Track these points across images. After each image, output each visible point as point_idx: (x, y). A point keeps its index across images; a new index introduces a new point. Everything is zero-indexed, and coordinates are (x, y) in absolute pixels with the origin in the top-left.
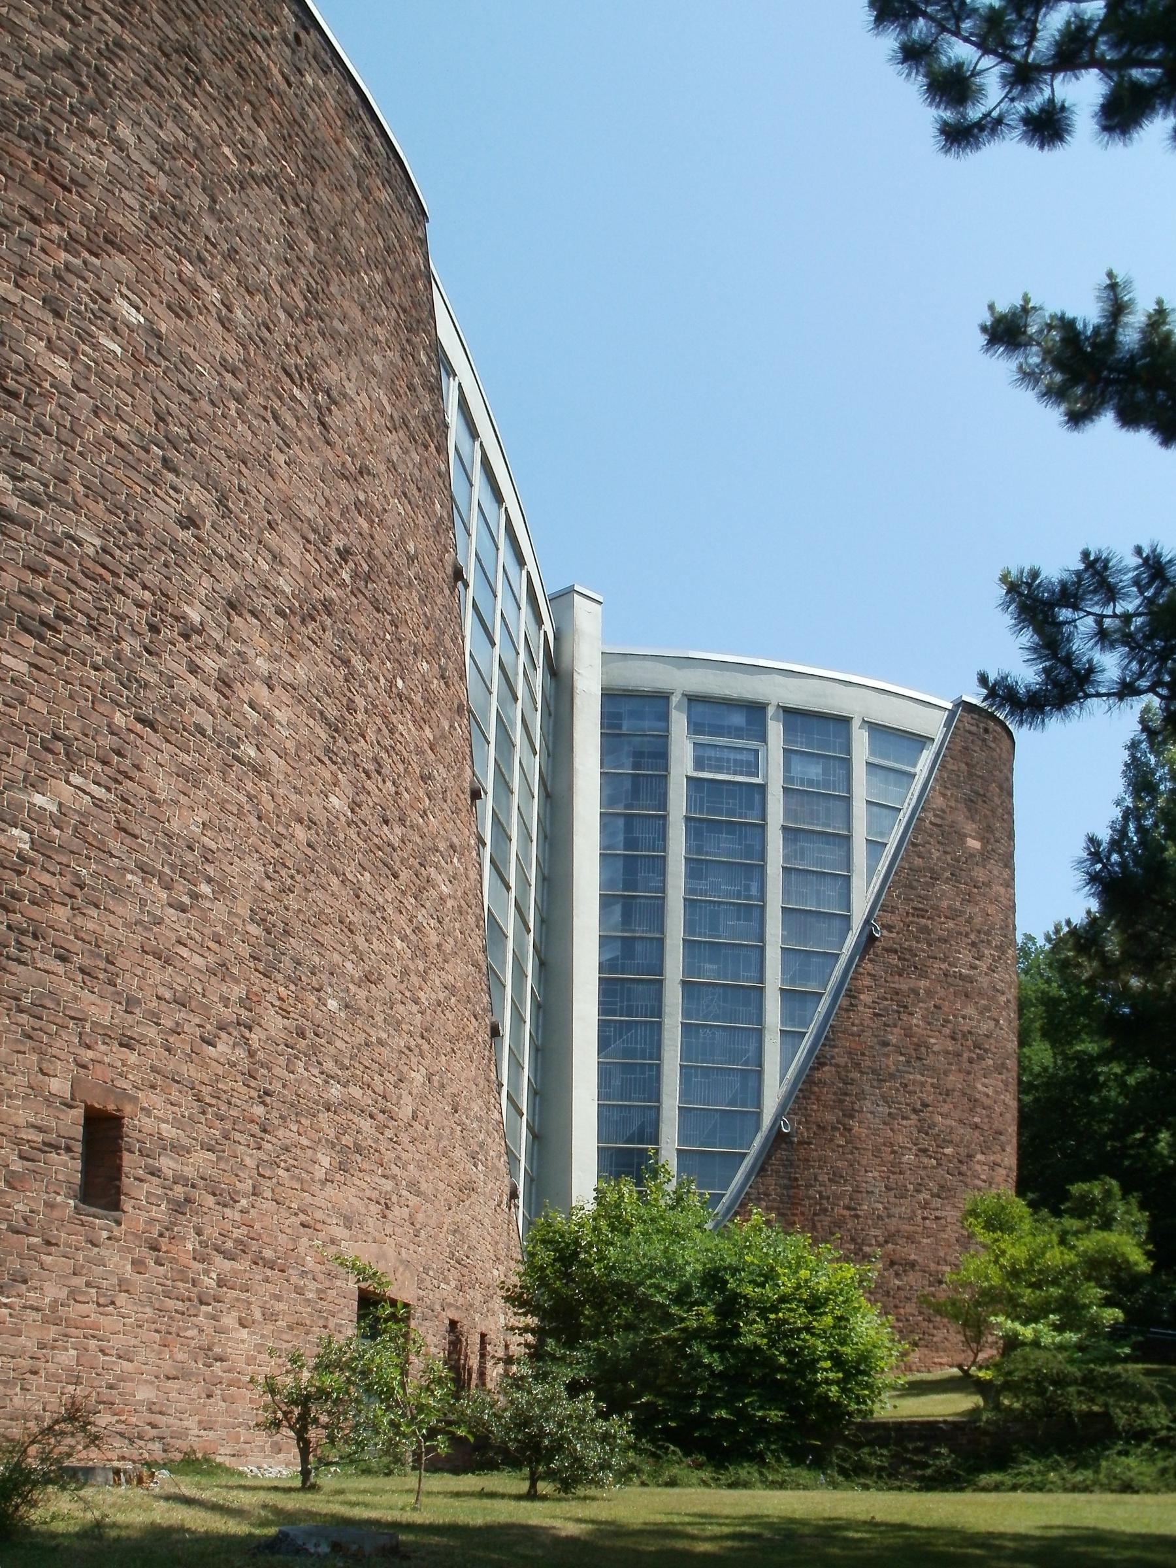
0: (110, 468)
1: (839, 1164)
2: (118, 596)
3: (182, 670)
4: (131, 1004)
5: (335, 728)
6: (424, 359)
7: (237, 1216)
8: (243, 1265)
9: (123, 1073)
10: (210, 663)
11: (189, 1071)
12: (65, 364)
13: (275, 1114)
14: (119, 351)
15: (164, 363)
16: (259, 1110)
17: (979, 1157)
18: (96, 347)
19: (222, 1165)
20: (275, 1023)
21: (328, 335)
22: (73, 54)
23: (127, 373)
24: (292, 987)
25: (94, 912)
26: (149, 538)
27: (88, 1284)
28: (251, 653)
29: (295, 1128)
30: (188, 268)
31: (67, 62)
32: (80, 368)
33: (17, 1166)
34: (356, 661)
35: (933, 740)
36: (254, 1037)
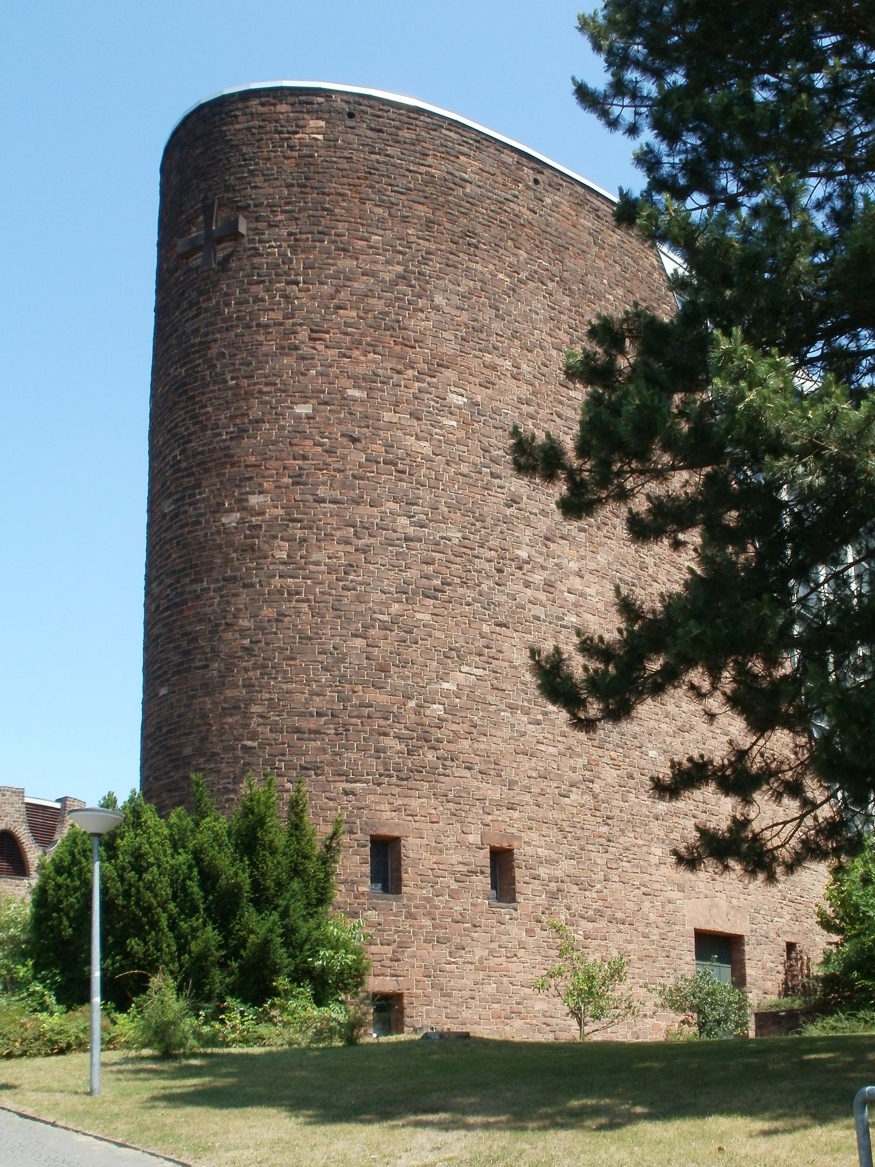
0: (460, 492)
2: (477, 561)
3: (520, 587)
4: (511, 785)
7: (595, 895)
8: (601, 924)
9: (510, 826)
10: (538, 578)
11: (552, 815)
12: (427, 444)
14: (455, 423)
15: (482, 418)
16: (605, 829)
19: (581, 866)
20: (610, 775)
22: (405, 271)
23: (461, 434)
24: (621, 750)
25: (484, 739)
26: (489, 521)
27: (500, 946)
29: (632, 835)
32: (435, 443)
33: (455, 886)
36: (596, 787)
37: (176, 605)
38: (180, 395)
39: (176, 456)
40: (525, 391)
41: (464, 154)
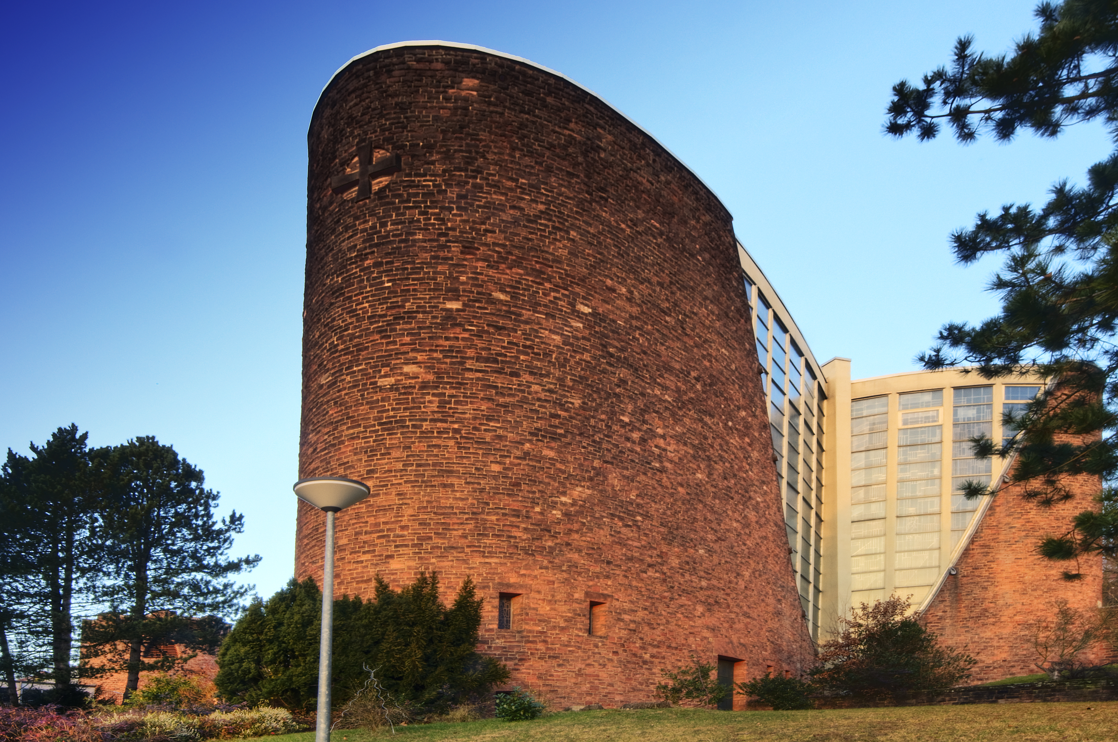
8: (663, 650)
10: (636, 435)
18: (571, 327)
20: (675, 562)
21: (683, 288)
28: (654, 429)
30: (609, 282)
34: (707, 419)
37: (334, 445)
38: (337, 297)
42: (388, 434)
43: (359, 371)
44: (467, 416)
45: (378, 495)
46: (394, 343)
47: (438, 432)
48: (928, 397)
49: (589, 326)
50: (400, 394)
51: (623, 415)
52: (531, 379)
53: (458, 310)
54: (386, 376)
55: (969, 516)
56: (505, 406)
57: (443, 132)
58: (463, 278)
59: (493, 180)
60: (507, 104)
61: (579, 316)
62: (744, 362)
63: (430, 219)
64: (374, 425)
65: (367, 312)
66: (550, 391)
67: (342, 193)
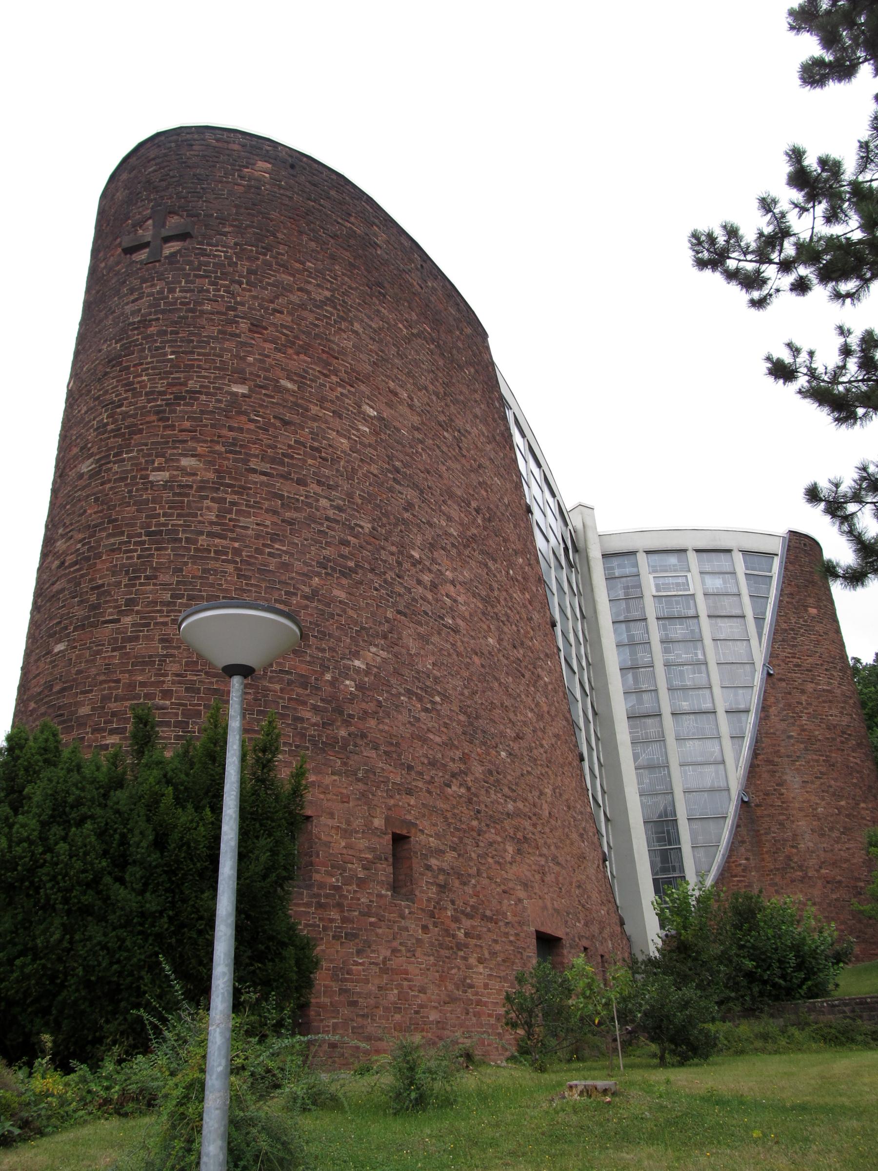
0: (371, 488)
1: (781, 817)
5: (486, 600)
6: (497, 405)
9: (410, 807)
11: (440, 804)
13: (483, 824)
16: (475, 823)
17: (862, 805)
18: (358, 430)
20: (478, 770)
21: (455, 402)
28: (443, 570)
30: (392, 384)
31: (330, 301)
34: (490, 564)
35: (777, 555)
37: (88, 559)
38: (114, 366)
39: (103, 419)
40: (416, 420)
41: (377, 226)
42: (157, 549)
43: (130, 459)
44: (250, 532)
45: (137, 638)
46: (172, 427)
47: (216, 552)
48: (673, 560)
49: (376, 433)
50: (175, 494)
51: (413, 549)
52: (319, 490)
53: (244, 395)
54: (159, 469)
55: (743, 716)
56: (291, 523)
57: (236, 206)
58: (250, 359)
59: (282, 259)
60: (296, 190)
61: (366, 418)
62: (514, 496)
63: (219, 290)
64: (140, 535)
65: (146, 386)
66: (340, 509)
67: (131, 254)
